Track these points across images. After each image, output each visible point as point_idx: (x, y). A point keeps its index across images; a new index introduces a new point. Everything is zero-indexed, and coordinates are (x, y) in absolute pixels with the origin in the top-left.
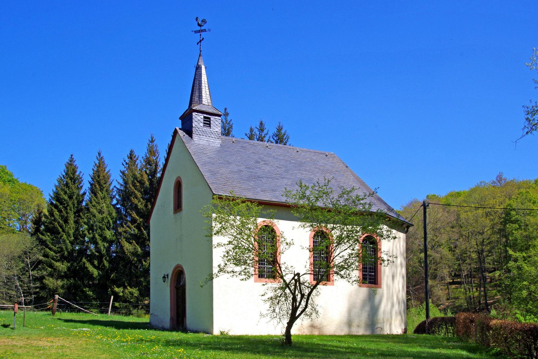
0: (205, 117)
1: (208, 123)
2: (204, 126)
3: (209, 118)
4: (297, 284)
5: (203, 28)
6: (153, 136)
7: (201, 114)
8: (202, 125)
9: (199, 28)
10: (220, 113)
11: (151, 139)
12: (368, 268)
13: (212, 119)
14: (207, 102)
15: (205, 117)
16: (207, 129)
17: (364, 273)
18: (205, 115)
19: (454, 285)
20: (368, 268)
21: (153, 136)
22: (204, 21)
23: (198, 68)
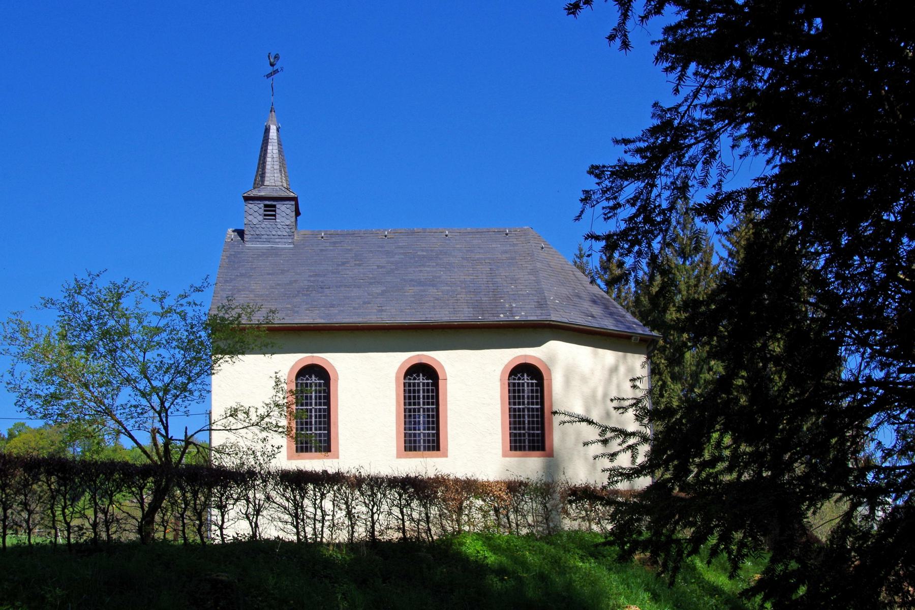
0: (266, 206)
1: (274, 213)
2: (265, 219)
3: (274, 206)
4: (165, 485)
5: (275, 68)
6: (581, 246)
7: (259, 202)
8: (261, 218)
9: (271, 69)
10: (292, 194)
11: (578, 253)
12: (526, 422)
13: (277, 206)
14: (273, 181)
15: (266, 206)
16: (271, 223)
17: (313, 449)
18: (267, 203)
19: (871, 415)
20: (526, 422)
21: (581, 246)
22: (277, 57)
23: (267, 130)
